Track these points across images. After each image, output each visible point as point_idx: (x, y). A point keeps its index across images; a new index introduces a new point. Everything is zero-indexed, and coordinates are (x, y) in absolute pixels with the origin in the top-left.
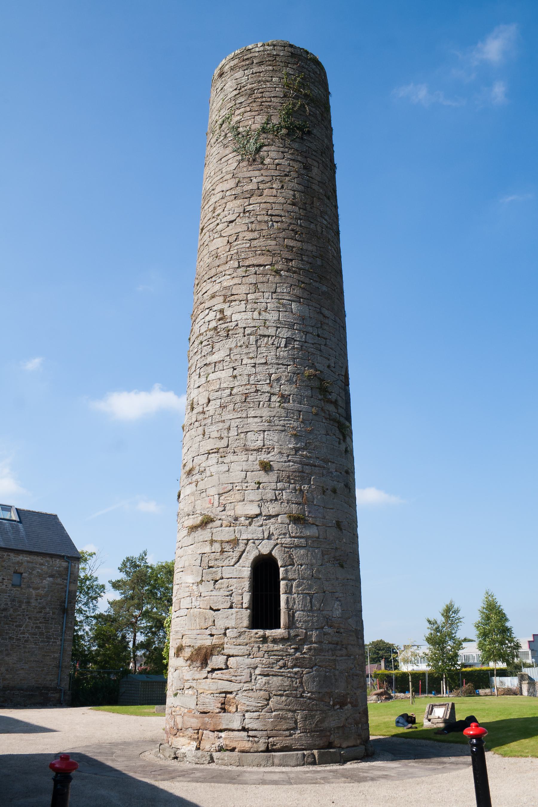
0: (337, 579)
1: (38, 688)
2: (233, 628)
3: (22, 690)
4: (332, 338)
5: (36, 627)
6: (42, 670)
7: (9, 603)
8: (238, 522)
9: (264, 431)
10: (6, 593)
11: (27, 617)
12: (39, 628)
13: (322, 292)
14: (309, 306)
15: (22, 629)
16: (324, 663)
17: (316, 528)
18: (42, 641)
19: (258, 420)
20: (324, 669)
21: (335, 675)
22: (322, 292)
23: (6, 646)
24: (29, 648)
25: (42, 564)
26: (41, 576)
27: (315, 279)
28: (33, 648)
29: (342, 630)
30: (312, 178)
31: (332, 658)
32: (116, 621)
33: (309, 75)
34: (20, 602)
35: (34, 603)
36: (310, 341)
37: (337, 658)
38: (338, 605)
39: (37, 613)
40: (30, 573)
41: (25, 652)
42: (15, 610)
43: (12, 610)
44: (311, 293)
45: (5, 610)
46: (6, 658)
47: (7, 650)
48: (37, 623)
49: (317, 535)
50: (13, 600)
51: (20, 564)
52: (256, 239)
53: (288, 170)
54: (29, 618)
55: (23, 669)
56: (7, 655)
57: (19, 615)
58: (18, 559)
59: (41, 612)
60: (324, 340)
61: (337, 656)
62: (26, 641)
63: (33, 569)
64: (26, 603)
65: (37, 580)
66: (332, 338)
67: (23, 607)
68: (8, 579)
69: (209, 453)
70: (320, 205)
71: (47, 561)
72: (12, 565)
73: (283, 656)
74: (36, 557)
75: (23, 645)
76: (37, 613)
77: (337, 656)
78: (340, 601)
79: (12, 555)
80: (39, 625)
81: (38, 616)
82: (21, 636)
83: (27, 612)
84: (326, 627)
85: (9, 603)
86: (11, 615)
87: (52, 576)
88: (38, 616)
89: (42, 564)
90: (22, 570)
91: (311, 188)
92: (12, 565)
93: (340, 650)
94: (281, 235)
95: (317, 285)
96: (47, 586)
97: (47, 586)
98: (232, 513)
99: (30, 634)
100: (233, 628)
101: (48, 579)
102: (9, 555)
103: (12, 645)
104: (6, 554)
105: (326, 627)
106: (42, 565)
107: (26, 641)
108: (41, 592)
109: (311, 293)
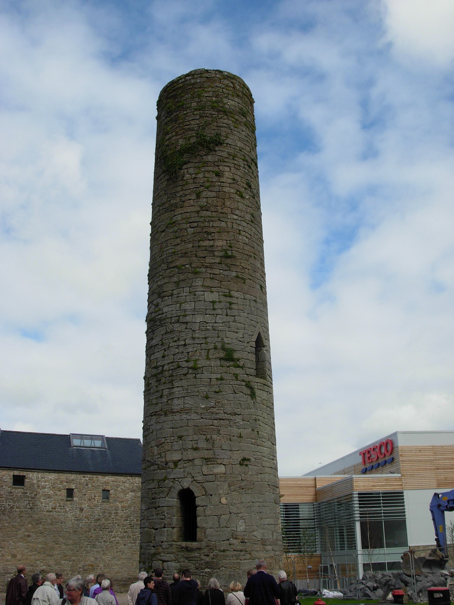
0: (242, 503)
3: (117, 580)
5: (124, 532)
6: (132, 565)
7: (101, 514)
8: (167, 466)
9: (184, 397)
10: (98, 506)
11: (116, 525)
12: (126, 532)
13: (231, 278)
14: (219, 292)
15: (113, 534)
16: (229, 565)
17: (224, 466)
18: (130, 543)
20: (230, 569)
22: (231, 278)
23: (102, 547)
24: (121, 548)
25: (124, 482)
27: (224, 269)
28: (123, 548)
29: (246, 541)
30: (223, 182)
31: (236, 561)
34: (110, 513)
35: (120, 513)
36: (220, 321)
37: (241, 561)
38: (242, 522)
39: (124, 520)
40: (116, 490)
41: (117, 552)
42: (107, 520)
43: (103, 519)
44: (221, 282)
45: (98, 520)
46: (103, 557)
47: (103, 551)
48: (124, 529)
49: (224, 472)
51: (107, 483)
52: (178, 244)
53: (202, 181)
54: (118, 525)
55: (117, 564)
57: (110, 523)
59: (127, 520)
60: (233, 317)
61: (241, 560)
62: (117, 543)
63: (117, 486)
64: (114, 513)
65: (122, 495)
67: (113, 517)
68: (98, 496)
69: (152, 416)
70: (230, 204)
72: (100, 485)
73: (197, 561)
74: (119, 477)
75: (115, 547)
76: (124, 520)
77: (241, 560)
78: (244, 519)
79: (100, 477)
80: (126, 530)
82: (113, 539)
83: (116, 520)
84: (232, 539)
85: (101, 514)
86: (103, 524)
89: (124, 482)
90: (108, 488)
91: (222, 191)
92: (100, 485)
93: (244, 555)
94: (196, 239)
95: (226, 273)
96: (130, 500)
97: (130, 500)
99: (120, 537)
100: (166, 542)
101: (130, 493)
102: (98, 477)
103: (107, 547)
104: (95, 476)
105: (232, 539)
106: (125, 482)
107: (117, 543)
109: (221, 282)
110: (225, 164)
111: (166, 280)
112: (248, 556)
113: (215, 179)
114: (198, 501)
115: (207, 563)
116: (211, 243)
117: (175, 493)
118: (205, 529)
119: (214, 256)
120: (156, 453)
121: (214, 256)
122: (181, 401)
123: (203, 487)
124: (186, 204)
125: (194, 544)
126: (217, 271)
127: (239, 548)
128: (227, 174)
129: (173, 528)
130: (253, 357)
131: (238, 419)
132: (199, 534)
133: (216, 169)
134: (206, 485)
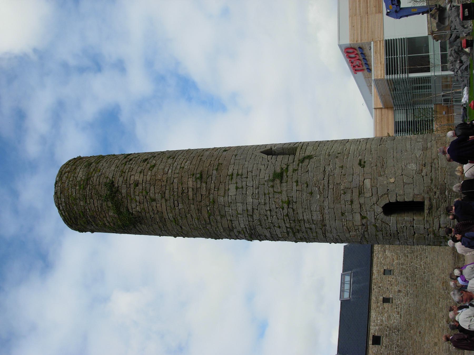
1: (453, 254)
2: (424, 225)
3: (455, 263)
4: (246, 166)
5: (417, 258)
11: (411, 264)
12: (417, 256)
14: (229, 184)
17: (365, 180)
18: (425, 253)
19: (305, 214)
21: (450, 168)
23: (429, 275)
26: (385, 258)
29: (424, 163)
31: (440, 171)
32: (435, 346)
33: (72, 181)
35: (402, 261)
36: (252, 183)
40: (384, 265)
45: (407, 278)
46: (436, 274)
49: (370, 180)
50: (401, 273)
51: (378, 272)
53: (142, 197)
54: (412, 263)
56: (434, 274)
57: (410, 269)
58: (376, 273)
59: (407, 256)
62: (425, 263)
63: (381, 263)
65: (388, 260)
66: (246, 166)
71: (376, 255)
81: (410, 257)
82: (422, 266)
86: (410, 274)
87: (385, 251)
88: (410, 257)
93: (435, 164)
94: (187, 202)
95: (214, 178)
97: (391, 254)
98: (360, 227)
99: (421, 261)
100: (424, 225)
101: (386, 253)
107: (425, 263)
108: (395, 258)
110: (128, 179)
111: (219, 225)
112: (436, 161)
113: (140, 187)
114: (393, 200)
115: (441, 193)
116: (190, 190)
117: (386, 218)
118: (414, 195)
119: (200, 188)
120: (355, 233)
121: (200, 188)
122: (314, 214)
123: (382, 196)
124: (160, 209)
125: (427, 203)
126: (213, 185)
127: (429, 168)
128: (137, 178)
129: (414, 220)
130: (280, 157)
131: (328, 169)
132: (419, 199)
133: (132, 186)
134: (380, 194)
